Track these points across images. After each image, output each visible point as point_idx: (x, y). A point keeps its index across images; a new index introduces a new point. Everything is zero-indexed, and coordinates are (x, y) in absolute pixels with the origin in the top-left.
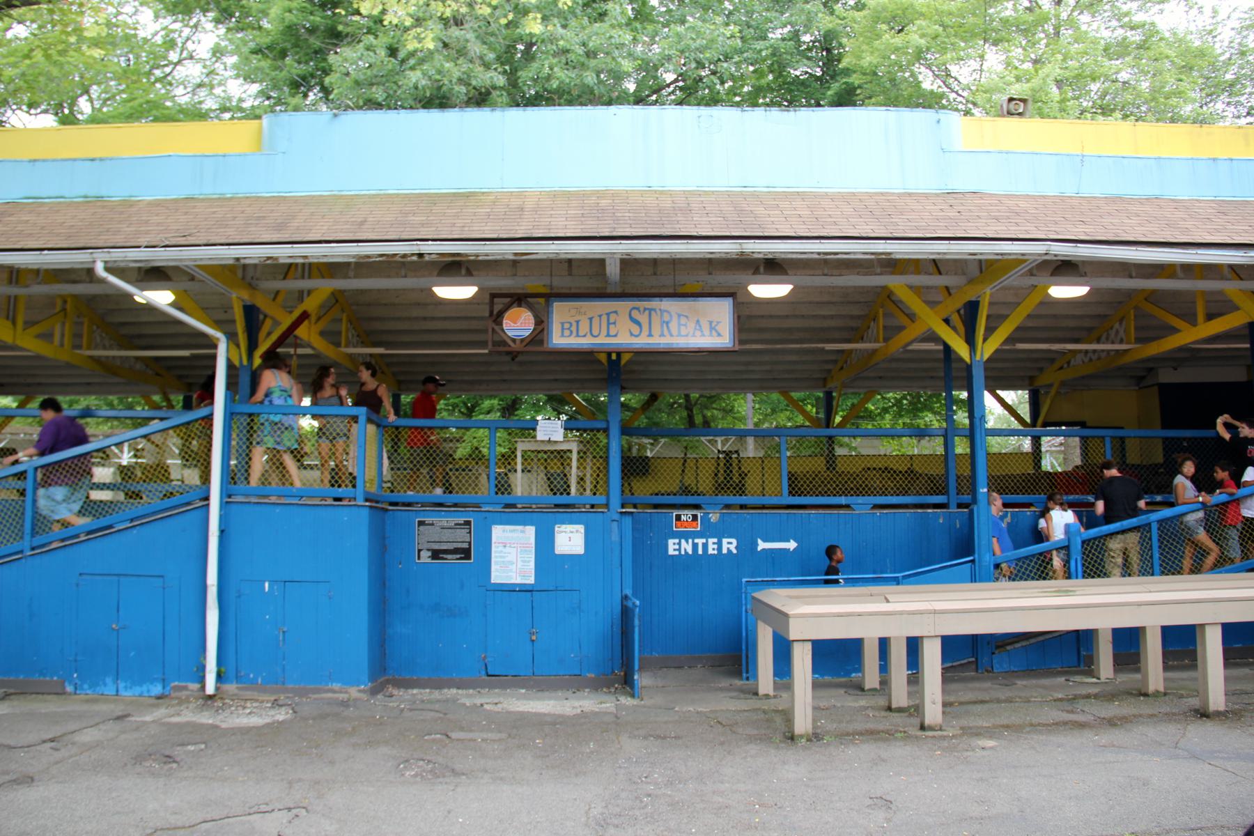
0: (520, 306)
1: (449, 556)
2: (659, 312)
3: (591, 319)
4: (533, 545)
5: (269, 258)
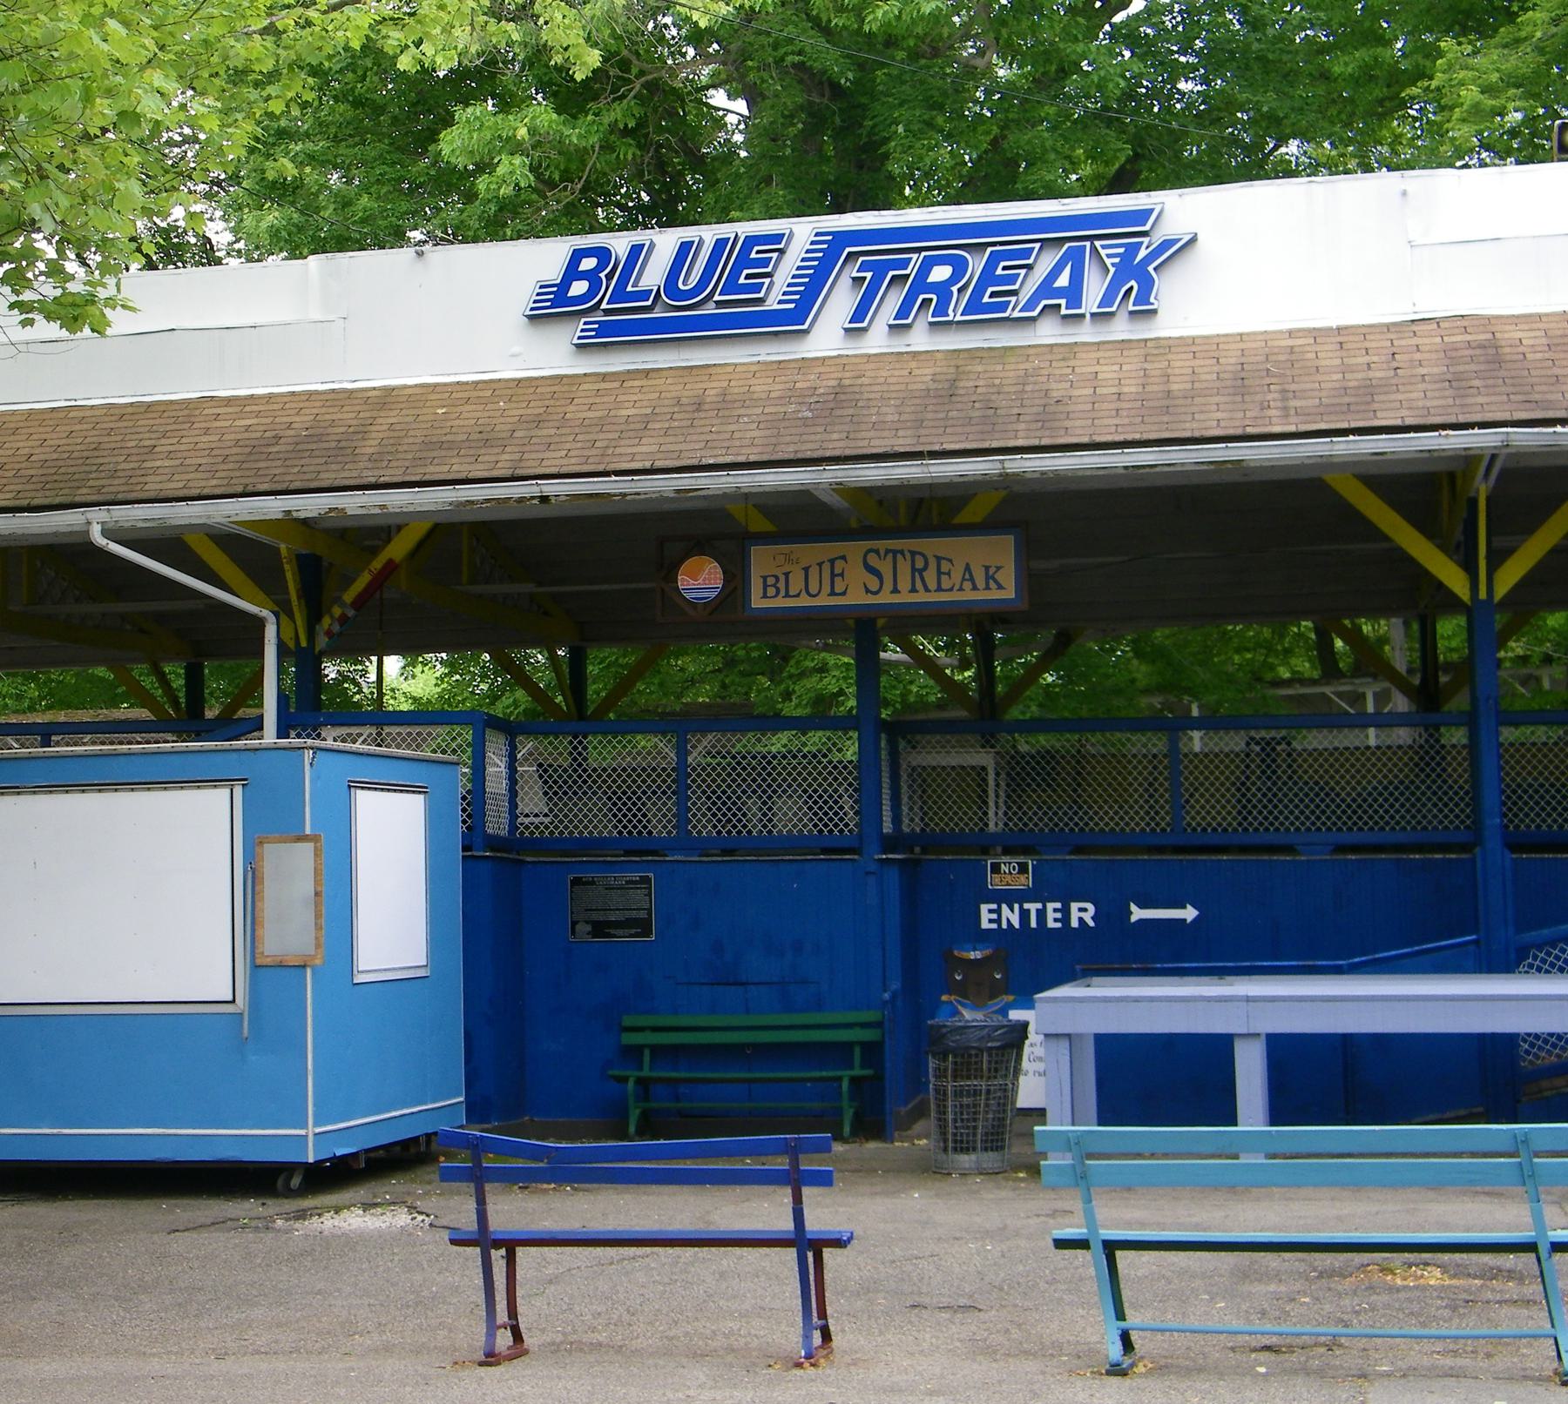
3: (806, 570)
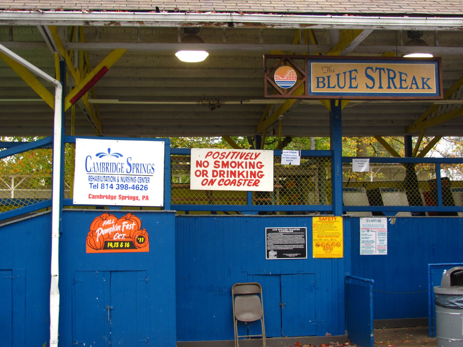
0: (285, 64)
1: (290, 255)
3: (338, 75)
4: (386, 230)
5: (112, 22)
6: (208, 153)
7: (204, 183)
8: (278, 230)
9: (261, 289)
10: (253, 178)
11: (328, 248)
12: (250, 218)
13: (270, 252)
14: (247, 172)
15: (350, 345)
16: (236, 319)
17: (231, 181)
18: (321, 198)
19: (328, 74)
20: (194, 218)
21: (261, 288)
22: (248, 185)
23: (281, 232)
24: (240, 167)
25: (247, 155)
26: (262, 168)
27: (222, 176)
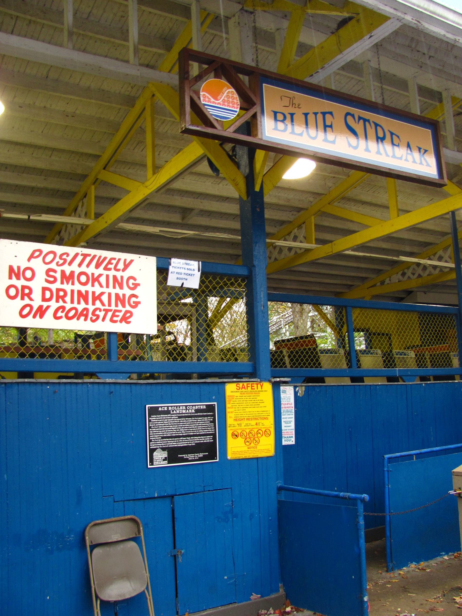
1: (191, 456)
2: (373, 125)
3: (306, 115)
4: (293, 405)
6: (35, 251)
7: (25, 312)
8: (168, 408)
9: (141, 528)
10: (120, 307)
11: (252, 439)
12: (118, 387)
13: (155, 454)
14: (110, 294)
15: (297, 612)
16: (97, 597)
17: (80, 311)
18: (200, 354)
19: (292, 110)
20: (3, 386)
21: (141, 525)
22: (112, 320)
23: (175, 412)
24: (96, 284)
25: (109, 263)
26: (136, 290)
27: (60, 300)
